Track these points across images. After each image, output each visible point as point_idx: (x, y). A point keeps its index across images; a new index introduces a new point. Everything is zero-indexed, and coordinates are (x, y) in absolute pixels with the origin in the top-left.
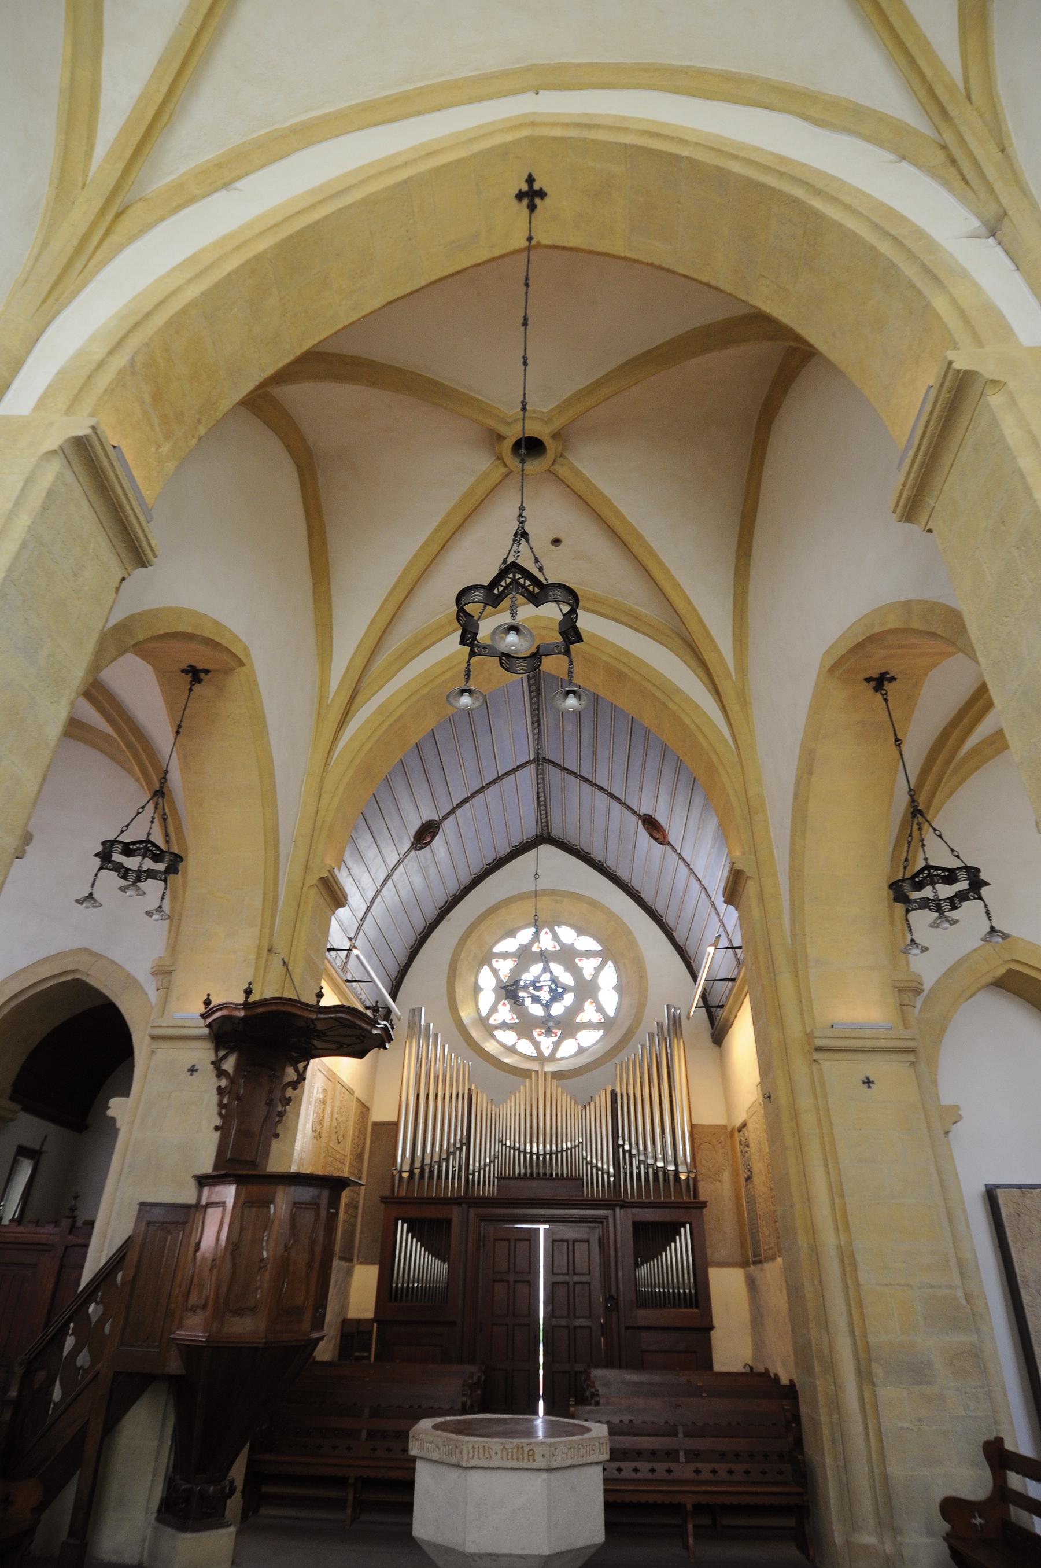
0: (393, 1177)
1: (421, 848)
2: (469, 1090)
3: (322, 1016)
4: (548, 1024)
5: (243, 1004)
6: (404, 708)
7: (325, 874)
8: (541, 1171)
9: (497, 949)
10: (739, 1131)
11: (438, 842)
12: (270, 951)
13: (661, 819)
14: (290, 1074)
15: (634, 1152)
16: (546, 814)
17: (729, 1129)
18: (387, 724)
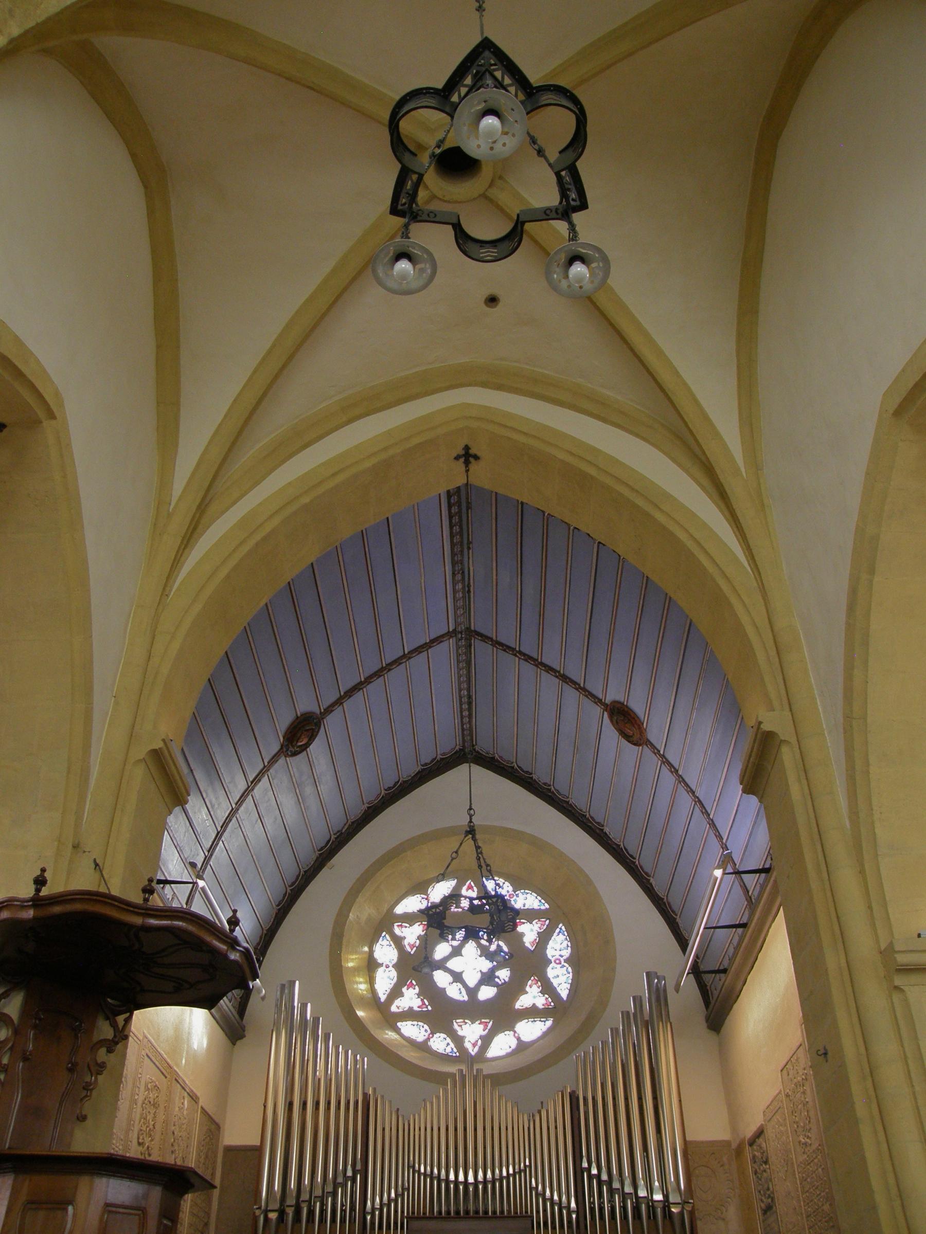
0: (255, 1219)
1: (295, 754)
2: (366, 1096)
3: (153, 922)
4: (472, 1009)
5: (32, 899)
6: (276, 521)
7: (158, 745)
8: (471, 1207)
9: (400, 909)
10: (751, 1145)
11: (317, 748)
12: (76, 847)
13: (637, 706)
14: (105, 1030)
15: (604, 1177)
16: (470, 716)
17: (734, 1145)
18: (251, 543)
